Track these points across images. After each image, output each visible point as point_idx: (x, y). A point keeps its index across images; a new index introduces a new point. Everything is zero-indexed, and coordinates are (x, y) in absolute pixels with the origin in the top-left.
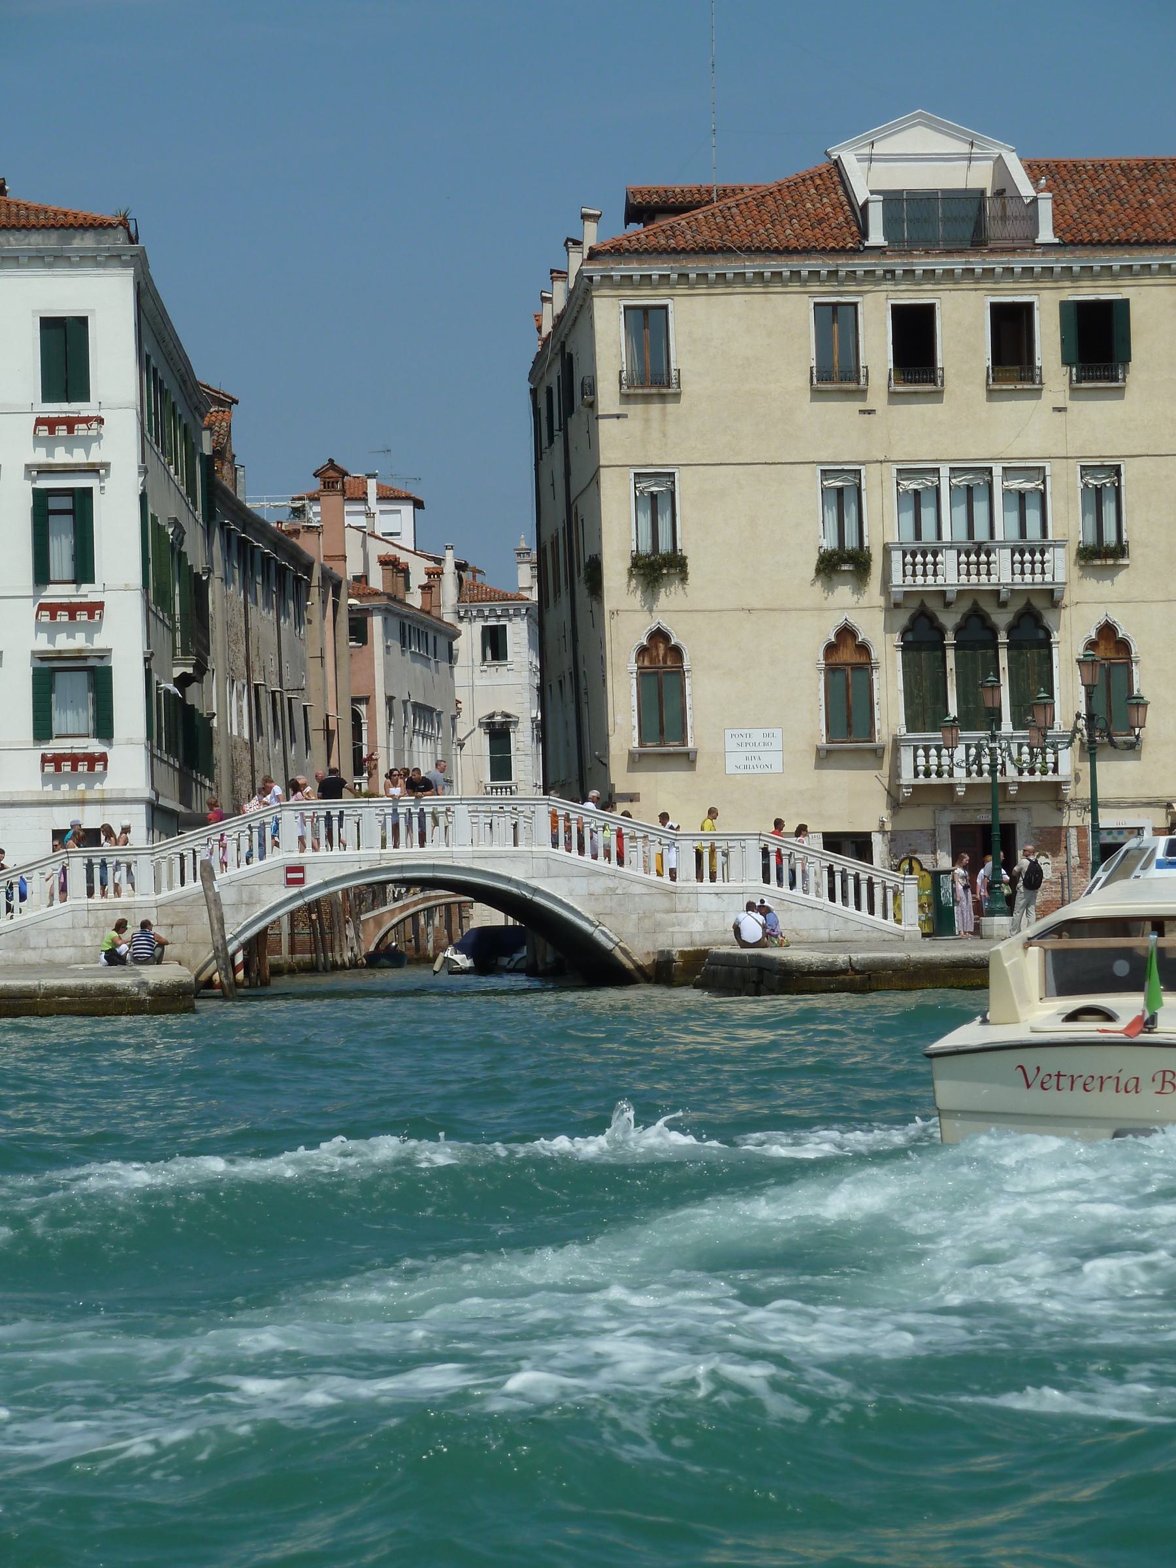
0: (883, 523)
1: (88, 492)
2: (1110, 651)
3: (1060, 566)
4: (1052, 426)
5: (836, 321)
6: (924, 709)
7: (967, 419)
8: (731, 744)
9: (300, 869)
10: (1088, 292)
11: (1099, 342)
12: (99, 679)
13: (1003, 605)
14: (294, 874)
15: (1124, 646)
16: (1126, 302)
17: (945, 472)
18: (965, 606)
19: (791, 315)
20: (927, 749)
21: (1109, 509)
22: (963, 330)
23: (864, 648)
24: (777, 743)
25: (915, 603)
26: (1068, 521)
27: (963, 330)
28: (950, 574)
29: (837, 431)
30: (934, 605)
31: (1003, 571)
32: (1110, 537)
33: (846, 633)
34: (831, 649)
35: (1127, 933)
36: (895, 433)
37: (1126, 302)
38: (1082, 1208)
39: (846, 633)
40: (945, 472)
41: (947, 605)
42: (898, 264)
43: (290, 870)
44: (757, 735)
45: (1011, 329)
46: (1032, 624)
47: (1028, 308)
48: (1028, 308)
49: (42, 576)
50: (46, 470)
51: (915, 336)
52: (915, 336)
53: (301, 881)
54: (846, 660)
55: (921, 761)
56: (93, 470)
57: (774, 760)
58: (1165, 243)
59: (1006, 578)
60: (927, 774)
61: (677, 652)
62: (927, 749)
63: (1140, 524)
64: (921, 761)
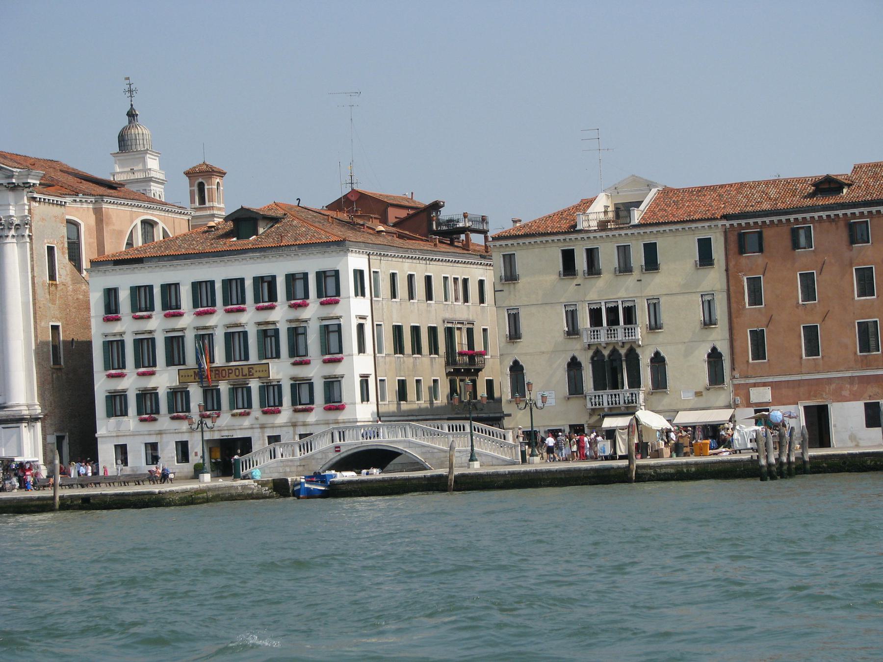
5: (568, 257)
6: (599, 385)
25: (594, 348)
29: (569, 290)
30: (600, 348)
46: (633, 357)
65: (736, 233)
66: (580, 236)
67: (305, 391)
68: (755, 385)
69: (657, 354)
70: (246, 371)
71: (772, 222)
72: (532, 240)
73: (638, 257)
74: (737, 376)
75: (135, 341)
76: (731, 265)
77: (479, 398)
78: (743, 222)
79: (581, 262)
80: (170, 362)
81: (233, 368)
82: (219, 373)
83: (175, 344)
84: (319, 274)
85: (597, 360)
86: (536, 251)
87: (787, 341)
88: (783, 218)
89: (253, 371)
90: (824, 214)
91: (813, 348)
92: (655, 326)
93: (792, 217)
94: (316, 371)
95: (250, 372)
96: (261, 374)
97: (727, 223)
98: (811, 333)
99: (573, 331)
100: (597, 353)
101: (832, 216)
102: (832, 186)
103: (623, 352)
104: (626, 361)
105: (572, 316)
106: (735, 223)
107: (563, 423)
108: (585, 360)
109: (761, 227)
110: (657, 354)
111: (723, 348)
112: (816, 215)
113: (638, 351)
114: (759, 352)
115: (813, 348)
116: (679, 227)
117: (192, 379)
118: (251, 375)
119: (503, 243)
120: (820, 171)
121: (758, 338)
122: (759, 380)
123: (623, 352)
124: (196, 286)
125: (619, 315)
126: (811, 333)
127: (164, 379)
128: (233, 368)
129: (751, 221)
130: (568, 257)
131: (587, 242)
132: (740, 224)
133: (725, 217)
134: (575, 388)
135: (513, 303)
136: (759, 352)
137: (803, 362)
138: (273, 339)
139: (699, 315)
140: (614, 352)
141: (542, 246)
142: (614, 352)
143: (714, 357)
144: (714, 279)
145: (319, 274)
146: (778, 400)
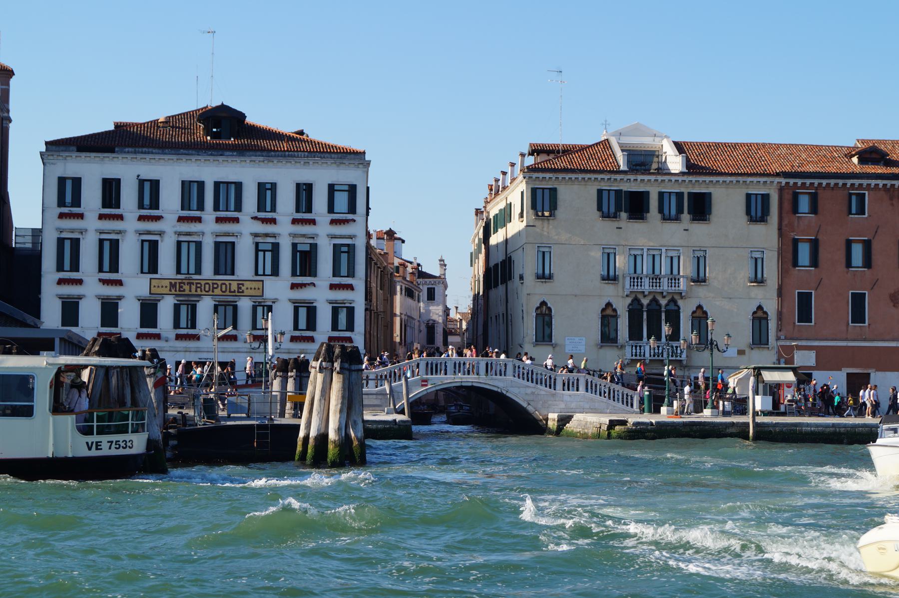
1: (118, 240)
2: (700, 317)
6: (635, 334)
8: (567, 342)
9: (426, 381)
10: (697, 190)
13: (664, 297)
14: (424, 382)
16: (710, 194)
17: (645, 250)
18: (650, 297)
20: (636, 347)
21: (344, 258)
23: (615, 310)
24: (584, 342)
25: (633, 296)
26: (686, 269)
28: (646, 287)
32: (547, 272)
34: (603, 310)
37: (710, 194)
39: (609, 305)
40: (645, 250)
41: (645, 296)
42: (632, 177)
43: (423, 381)
44: (577, 339)
47: (648, 193)
48: (648, 193)
49: (101, 270)
50: (179, 234)
53: (426, 385)
54: (608, 316)
55: (634, 351)
56: (120, 232)
59: (666, 288)
60: (636, 355)
61: (550, 309)
62: (636, 347)
64: (634, 351)
65: (791, 192)
66: (666, 178)
67: (343, 317)
68: (799, 348)
69: (700, 307)
70: (234, 287)
71: (828, 184)
72: (573, 176)
74: (783, 337)
76: (785, 222)
78: (800, 182)
81: (219, 283)
84: (217, 185)
85: (635, 312)
87: (829, 306)
88: (841, 182)
89: (243, 288)
90: (881, 183)
91: (858, 316)
92: (699, 280)
93: (849, 182)
95: (239, 288)
96: (253, 292)
97: (784, 181)
98: (858, 301)
99: (610, 278)
100: (636, 301)
101: (888, 186)
102: (874, 156)
104: (647, 311)
106: (792, 181)
108: (622, 307)
109: (816, 189)
110: (700, 307)
111: (771, 307)
112: (873, 182)
113: (681, 303)
114: (805, 315)
115: (858, 316)
116: (734, 179)
117: (166, 291)
118: (240, 292)
119: (541, 175)
121: (805, 300)
122: (804, 343)
124: (186, 186)
126: (858, 301)
128: (219, 283)
129: (808, 182)
131: (633, 184)
132: (795, 184)
133: (786, 175)
134: (608, 338)
136: (805, 315)
137: (850, 328)
138: (269, 255)
139: (747, 271)
140: (654, 301)
141: (583, 183)
142: (654, 301)
143: (759, 318)
144: (766, 236)
145: (217, 185)
146: (821, 365)
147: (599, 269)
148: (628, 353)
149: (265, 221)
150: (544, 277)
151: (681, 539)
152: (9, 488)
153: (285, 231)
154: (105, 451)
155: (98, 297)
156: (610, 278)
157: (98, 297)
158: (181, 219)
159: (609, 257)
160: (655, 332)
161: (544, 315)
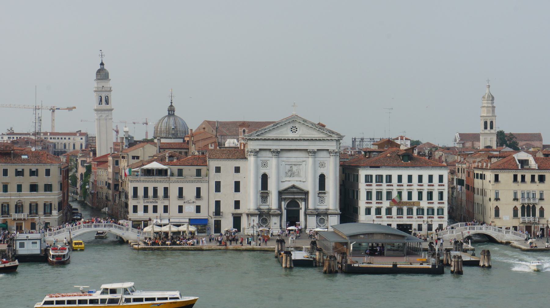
0: (519, 196)
2: (542, 210)
3: (537, 201)
4: (537, 187)
5: (515, 177)
6: (523, 215)
7: (529, 187)
10: (541, 174)
11: (542, 179)
12: (443, 210)
14: (469, 232)
15: (543, 209)
19: (511, 175)
22: (528, 178)
26: (538, 196)
27: (528, 178)
28: (526, 201)
29: (515, 187)
31: (532, 201)
33: (515, 207)
35: (517, 210)
36: (521, 187)
38: (128, 285)
39: (515, 207)
45: (533, 177)
46: (534, 207)
51: (523, 177)
52: (523, 177)
54: (515, 210)
57: (508, 219)
58: (548, 169)
63: (545, 197)
69: (542, 207)
73: (519, 178)
75: (387, 192)
77: (223, 232)
79: (519, 178)
80: (388, 199)
82: (405, 204)
83: (389, 194)
84: (376, 176)
85: (523, 207)
86: (506, 174)
92: (541, 199)
94: (436, 206)
99: (516, 199)
103: (531, 206)
105: (515, 194)
107: (511, 225)
110: (542, 207)
113: (536, 206)
120: (386, 137)
123: (531, 206)
124: (366, 176)
125: (530, 195)
127: (386, 204)
130: (515, 177)
134: (515, 215)
135: (497, 189)
145: (376, 176)
147: (513, 197)
148: (521, 220)
149: (420, 185)
150: (497, 199)
151: (483, 275)
152: (2, 278)
153: (426, 189)
154: (12, 265)
155: (233, 214)
156: (516, 199)
157: (233, 214)
158: (408, 185)
159: (515, 194)
160: (528, 215)
161: (497, 210)
